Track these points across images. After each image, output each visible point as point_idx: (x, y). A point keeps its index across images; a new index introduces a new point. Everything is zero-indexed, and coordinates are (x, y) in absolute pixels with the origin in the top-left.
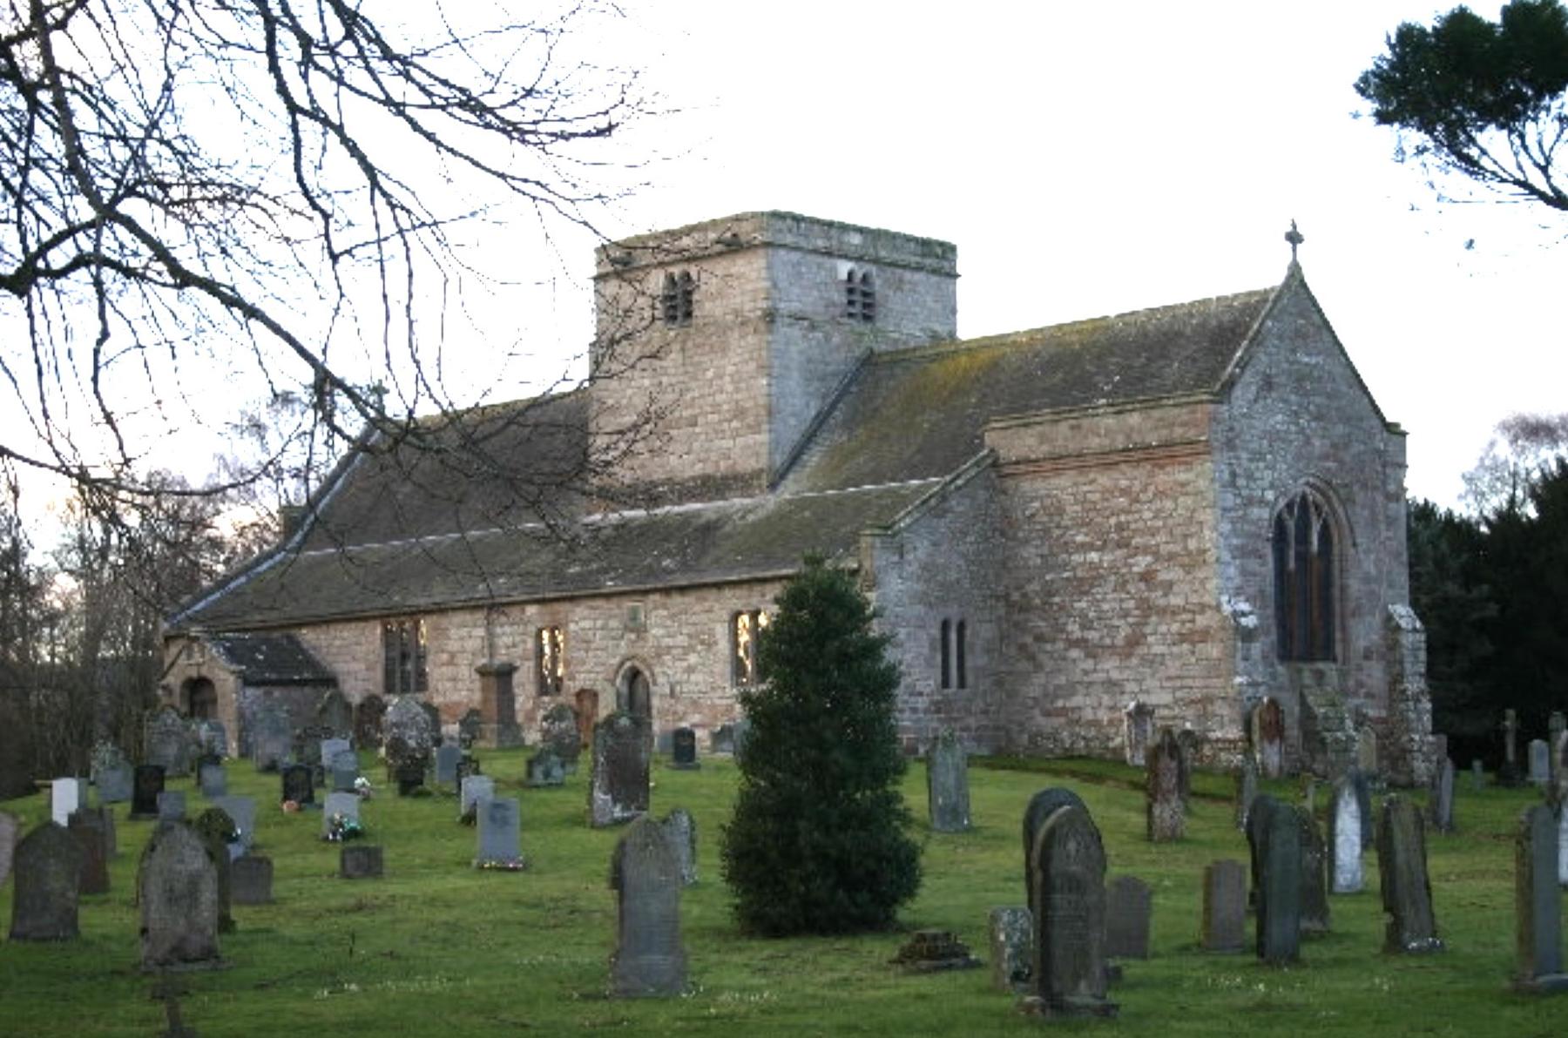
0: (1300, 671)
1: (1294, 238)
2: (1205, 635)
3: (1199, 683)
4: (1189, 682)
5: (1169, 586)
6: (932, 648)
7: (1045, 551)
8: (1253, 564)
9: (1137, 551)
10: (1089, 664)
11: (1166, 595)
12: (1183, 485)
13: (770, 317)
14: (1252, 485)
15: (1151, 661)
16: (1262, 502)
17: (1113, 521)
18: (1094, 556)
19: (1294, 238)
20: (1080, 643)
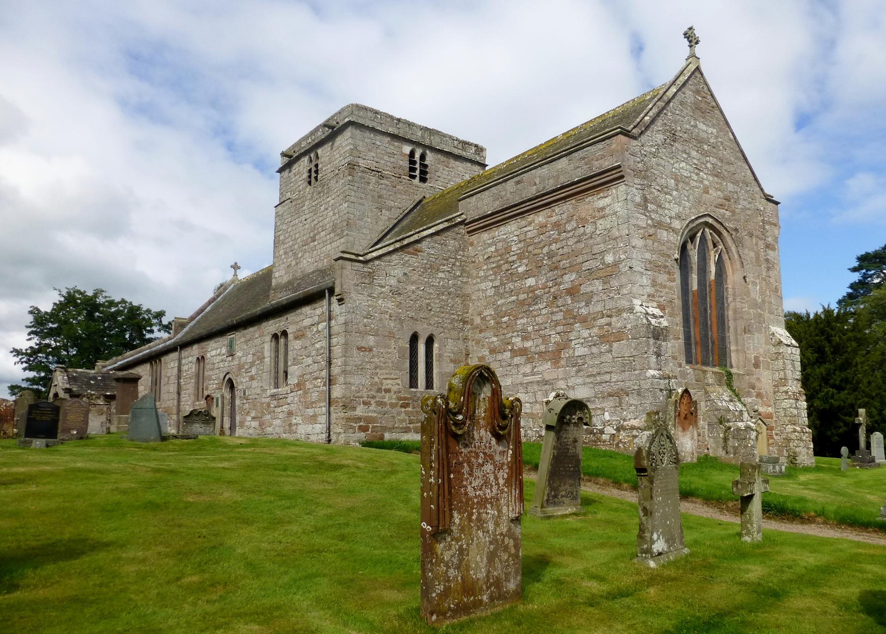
0: (705, 372)
1: (691, 38)
2: (619, 336)
3: (614, 377)
4: (607, 377)
5: (589, 299)
6: (402, 357)
7: (497, 283)
8: (662, 278)
9: (565, 271)
10: (527, 369)
11: (587, 305)
12: (603, 209)
13: (352, 166)
14: (660, 211)
15: (577, 364)
16: (669, 228)
17: (545, 250)
18: (531, 281)
19: (691, 38)
20: (523, 352)
